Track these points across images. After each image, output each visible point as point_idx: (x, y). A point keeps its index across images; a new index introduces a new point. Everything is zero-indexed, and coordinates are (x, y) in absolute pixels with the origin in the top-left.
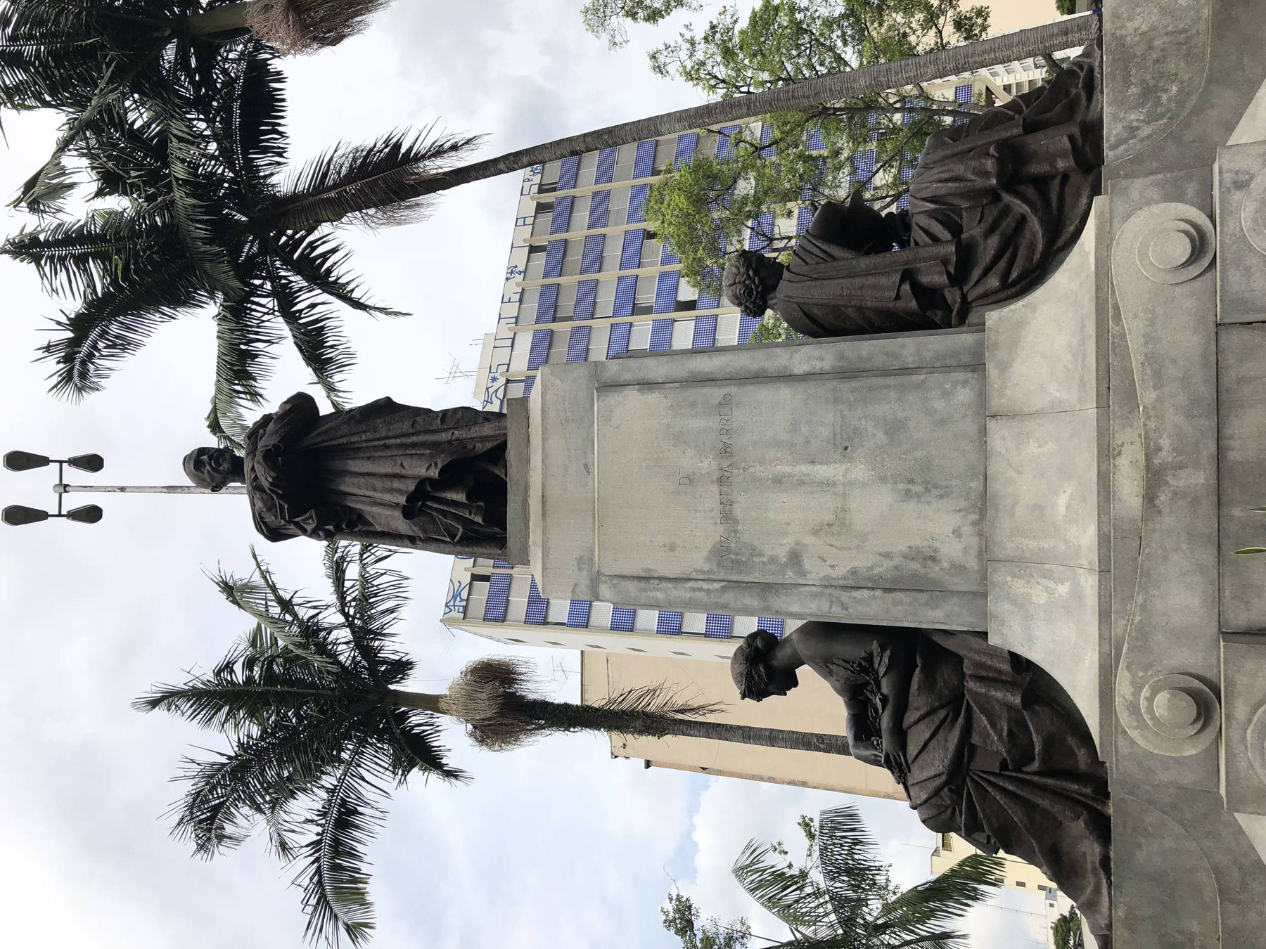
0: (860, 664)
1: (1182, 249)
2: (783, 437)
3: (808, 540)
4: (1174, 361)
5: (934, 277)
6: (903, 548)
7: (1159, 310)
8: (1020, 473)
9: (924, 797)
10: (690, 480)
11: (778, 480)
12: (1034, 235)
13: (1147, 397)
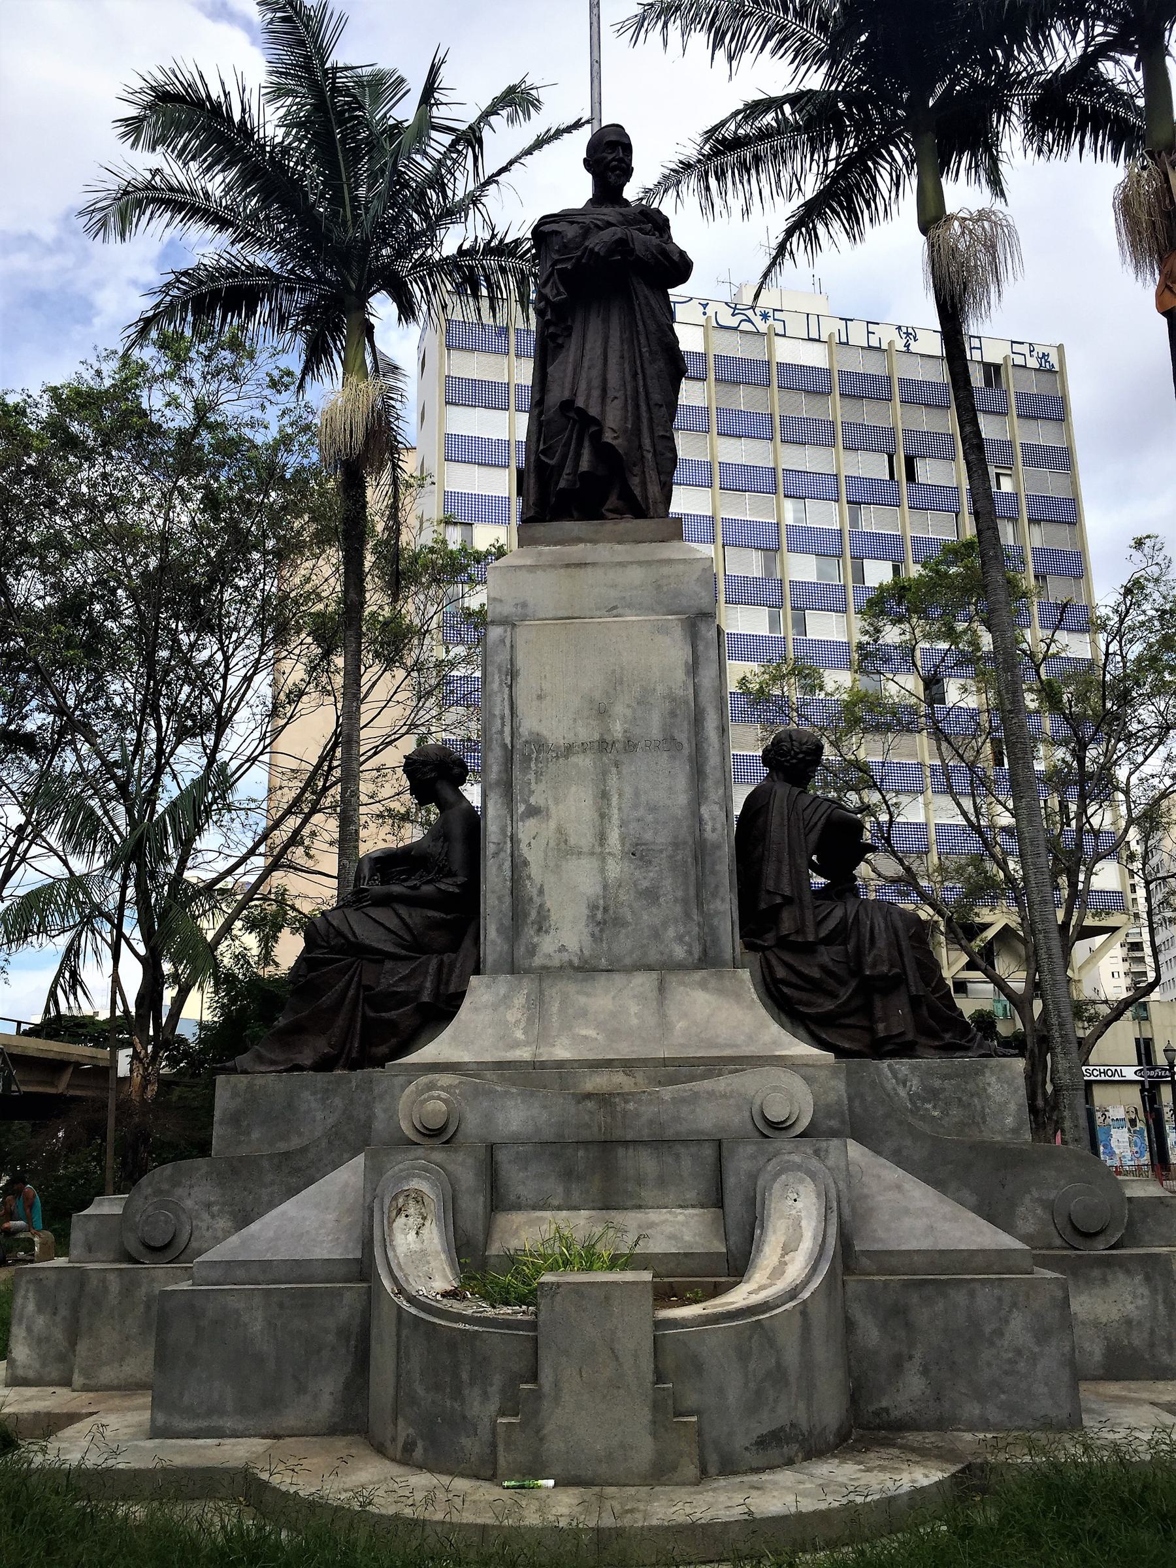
1: (776, 1113)
2: (643, 798)
3: (552, 824)
4: (693, 1111)
5: (787, 924)
6: (548, 905)
7: (732, 1101)
9: (335, 923)
10: (603, 713)
11: (604, 795)
12: (820, 1006)
13: (667, 1092)
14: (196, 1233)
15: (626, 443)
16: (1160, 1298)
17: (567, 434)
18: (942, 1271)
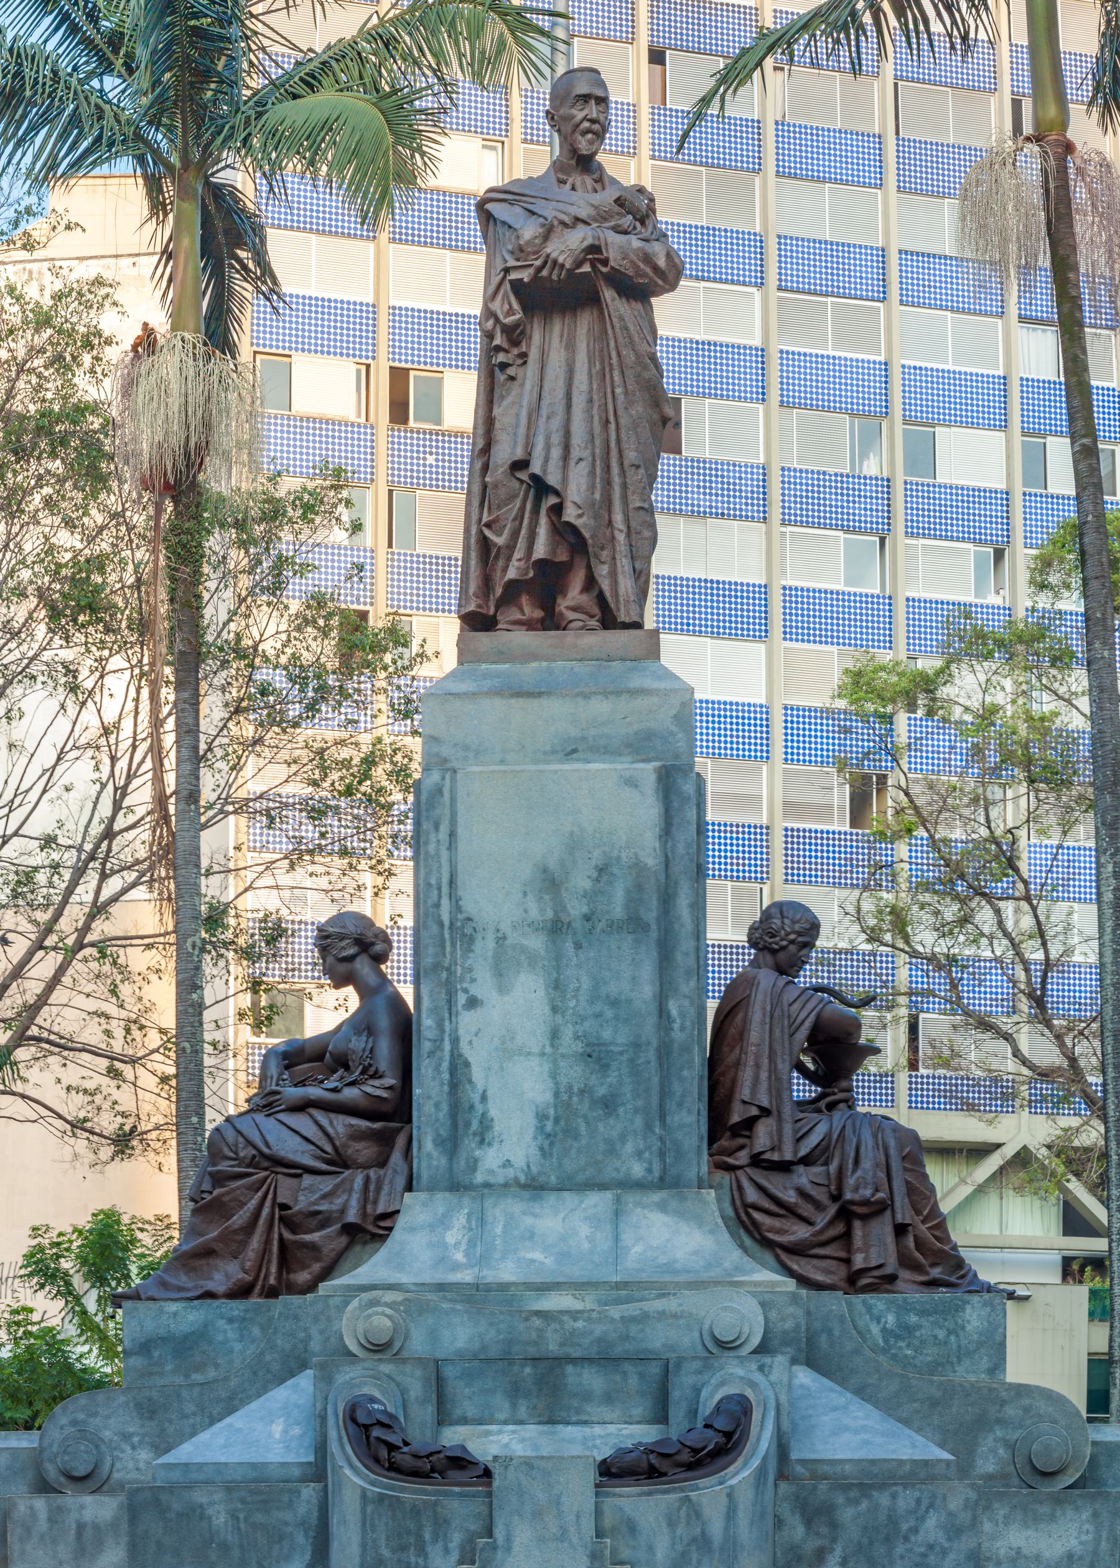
0: (370, 1065)
4: (642, 1330)
6: (493, 1113)
7: (682, 1321)
8: (564, 1219)
13: (615, 1312)
14: (118, 1465)
15: (592, 522)
16: (1104, 1534)
17: (518, 502)
18: (872, 1479)
